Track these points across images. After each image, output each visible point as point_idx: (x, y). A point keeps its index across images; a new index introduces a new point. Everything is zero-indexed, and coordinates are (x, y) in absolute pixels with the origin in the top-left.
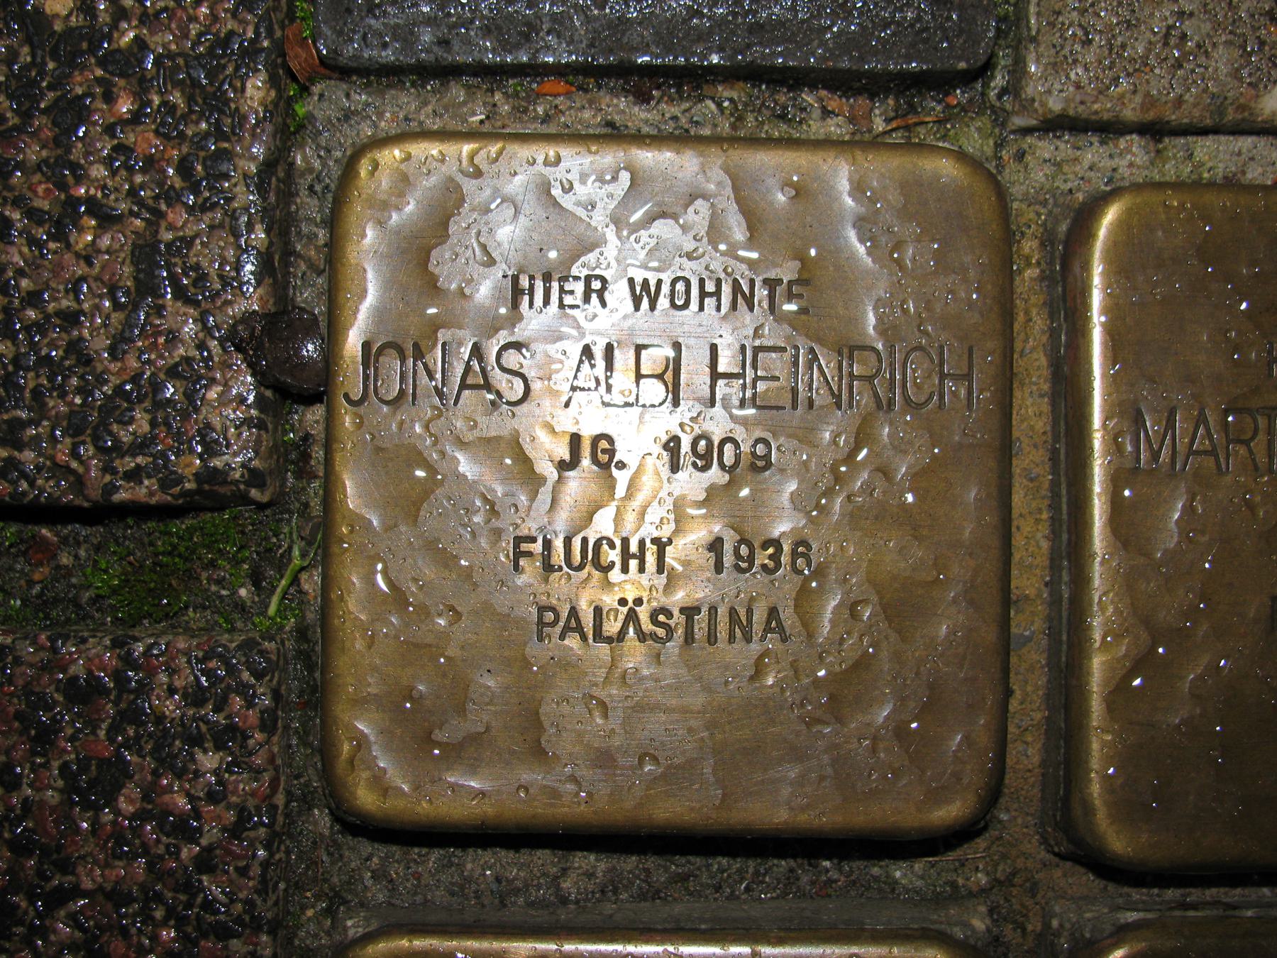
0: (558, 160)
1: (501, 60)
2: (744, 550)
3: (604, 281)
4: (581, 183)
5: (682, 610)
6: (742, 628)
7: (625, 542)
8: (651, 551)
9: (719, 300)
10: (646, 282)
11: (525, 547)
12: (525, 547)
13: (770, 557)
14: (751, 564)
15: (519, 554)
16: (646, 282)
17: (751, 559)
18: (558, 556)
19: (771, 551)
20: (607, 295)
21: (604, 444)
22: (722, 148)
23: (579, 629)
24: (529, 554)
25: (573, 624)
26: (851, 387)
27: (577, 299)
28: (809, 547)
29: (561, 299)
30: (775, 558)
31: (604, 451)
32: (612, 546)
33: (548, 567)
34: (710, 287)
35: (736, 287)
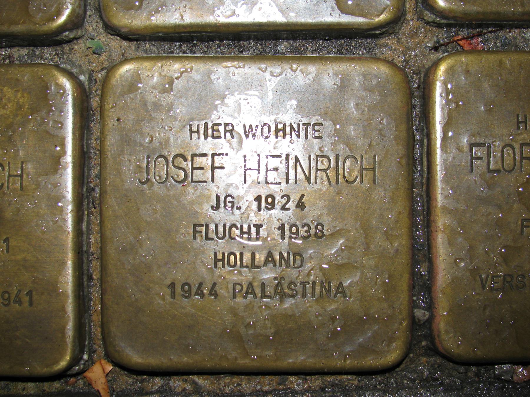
2: (294, 229)
5: (301, 283)
7: (242, 227)
8: (253, 230)
10: (251, 127)
11: (198, 229)
12: (198, 229)
13: (306, 232)
16: (251, 127)
17: (297, 233)
18: (212, 235)
19: (306, 228)
20: (239, 152)
23: (274, 261)
31: (229, 202)
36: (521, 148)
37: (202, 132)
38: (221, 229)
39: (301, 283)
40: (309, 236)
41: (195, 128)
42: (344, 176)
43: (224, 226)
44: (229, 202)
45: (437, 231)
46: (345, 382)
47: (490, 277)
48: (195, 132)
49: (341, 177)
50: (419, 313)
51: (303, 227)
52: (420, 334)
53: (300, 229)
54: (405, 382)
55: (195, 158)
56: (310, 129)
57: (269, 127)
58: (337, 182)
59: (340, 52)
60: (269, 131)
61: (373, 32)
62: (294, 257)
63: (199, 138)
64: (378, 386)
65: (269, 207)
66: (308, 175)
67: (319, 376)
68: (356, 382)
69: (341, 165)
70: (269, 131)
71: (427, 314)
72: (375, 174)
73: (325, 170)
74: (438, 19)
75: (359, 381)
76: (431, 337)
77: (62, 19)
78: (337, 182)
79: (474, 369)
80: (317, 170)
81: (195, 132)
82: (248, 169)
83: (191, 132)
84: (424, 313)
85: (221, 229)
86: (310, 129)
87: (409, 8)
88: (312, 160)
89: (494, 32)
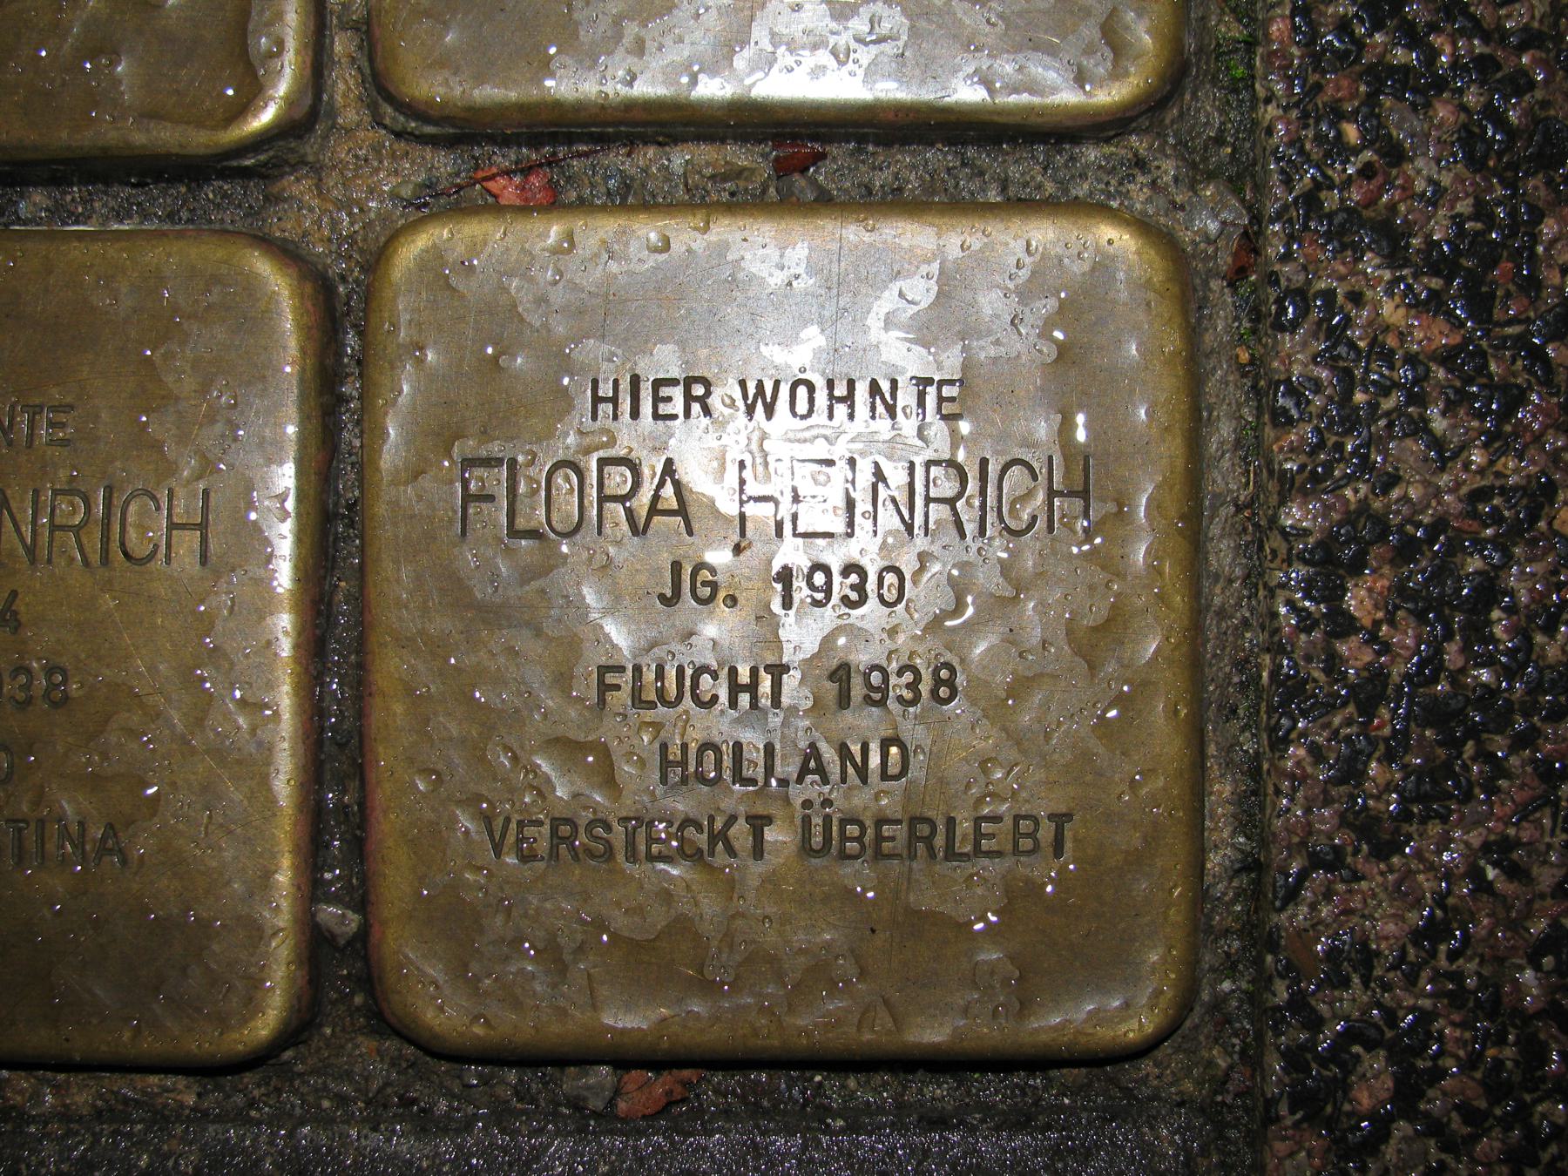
0: (750, 761)
1: (292, 364)
2: (819, 578)
3: (706, 383)
4: (791, 570)
6: (855, 765)
7: (733, 672)
9: (852, 407)
11: (610, 678)
12: (610, 678)
13: (908, 686)
14: (828, 597)
15: (604, 688)
19: (854, 578)
21: (705, 575)
22: (271, 55)
24: (617, 687)
25: (812, 764)
26: (1051, 505)
27: (678, 406)
28: (953, 671)
29: (655, 408)
30: (860, 588)
31: (704, 584)
32: (715, 676)
33: (638, 700)
34: (840, 391)
35: (875, 389)
36: (928, 472)
37: (625, 406)
38: (671, 673)
39: (1051, 817)
40: (29, 701)
41: (606, 390)
42: (123, 544)
43: (680, 671)
44: (704, 584)
45: (370, 694)
46: (158, 1095)
47: (513, 825)
48: (605, 400)
49: (991, 518)
50: (330, 913)
51: (900, 673)
52: (345, 972)
53: (893, 680)
54: (326, 1104)
55: (607, 469)
56: (931, 391)
57: (811, 388)
58: (982, 531)
59: (171, 217)
60: (811, 401)
61: (235, 163)
62: (885, 755)
63: (615, 417)
64: (253, 1113)
65: (819, 596)
66: (907, 517)
67: (86, 1075)
68: (191, 1100)
69: (116, 515)
70: (811, 401)
71: (353, 920)
72: (204, 541)
73: (951, 502)
74: (413, 125)
75: (199, 1095)
76: (369, 979)
77: (267, 116)
78: (982, 531)
79: (512, 1076)
80: (928, 500)
81: (605, 400)
82: (194, 527)
83: (597, 400)
84: (343, 915)
85: (671, 673)
86: (931, 391)
87: (345, 96)
88: (595, 483)
89: (586, 155)
